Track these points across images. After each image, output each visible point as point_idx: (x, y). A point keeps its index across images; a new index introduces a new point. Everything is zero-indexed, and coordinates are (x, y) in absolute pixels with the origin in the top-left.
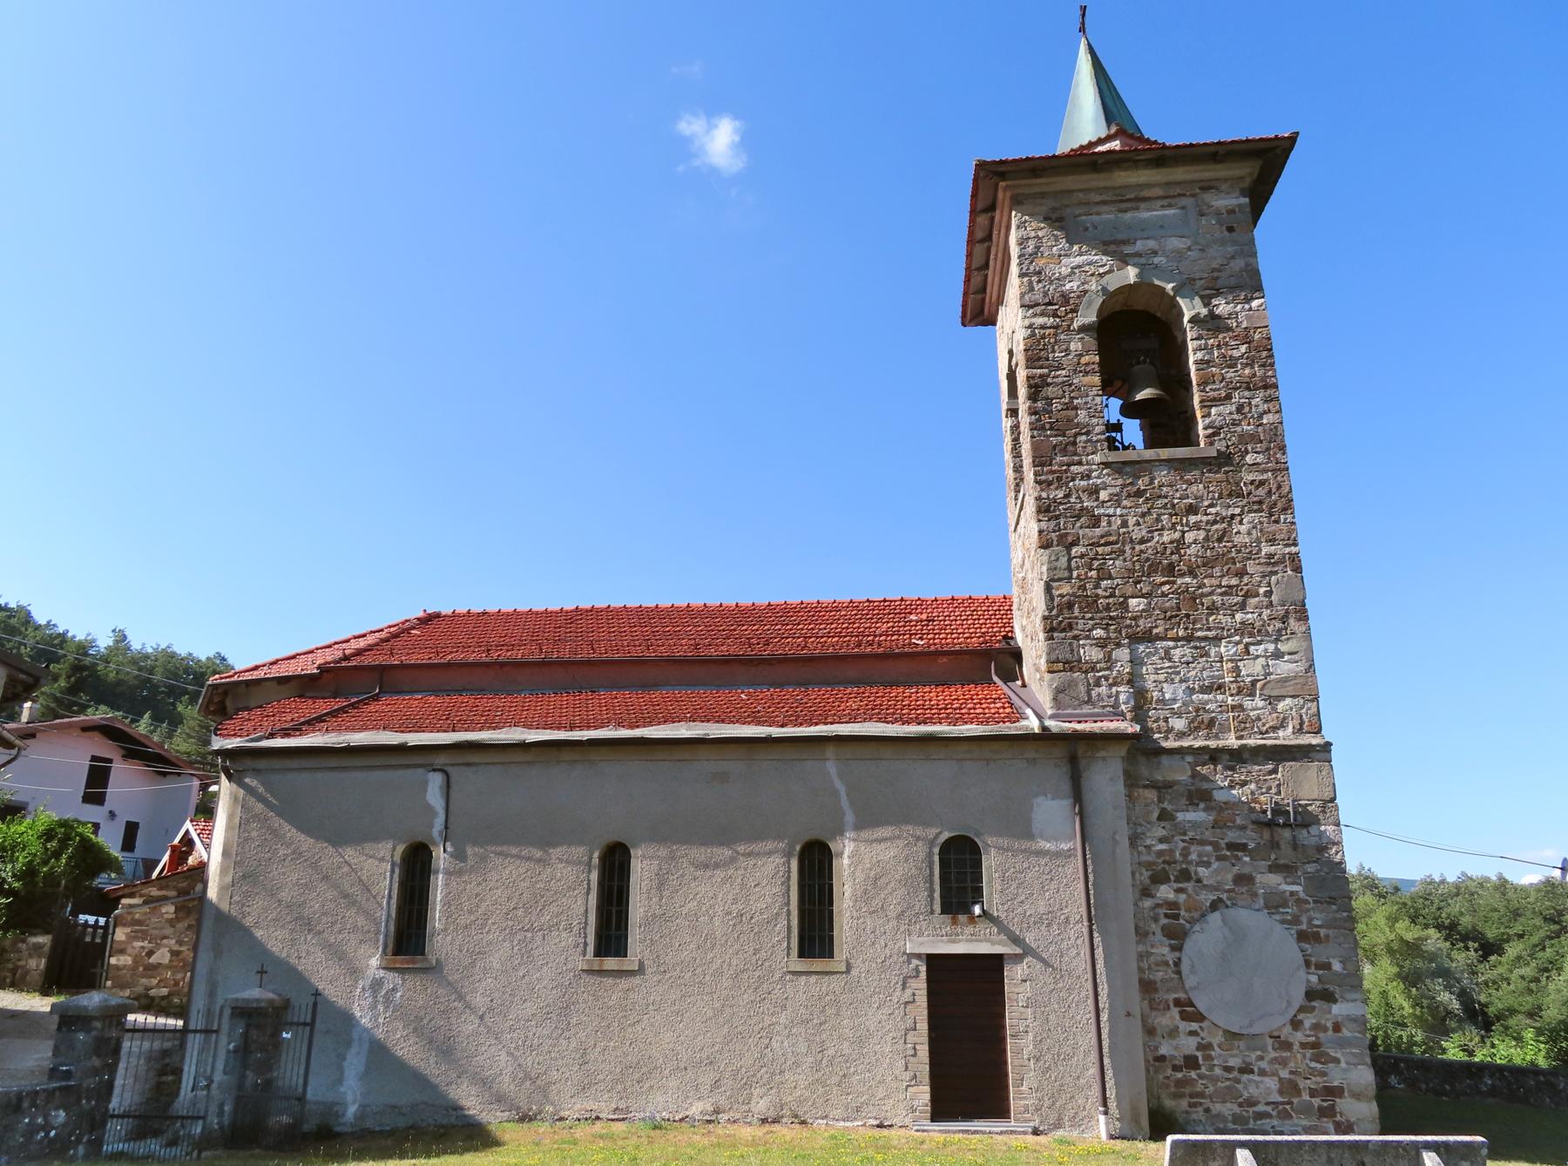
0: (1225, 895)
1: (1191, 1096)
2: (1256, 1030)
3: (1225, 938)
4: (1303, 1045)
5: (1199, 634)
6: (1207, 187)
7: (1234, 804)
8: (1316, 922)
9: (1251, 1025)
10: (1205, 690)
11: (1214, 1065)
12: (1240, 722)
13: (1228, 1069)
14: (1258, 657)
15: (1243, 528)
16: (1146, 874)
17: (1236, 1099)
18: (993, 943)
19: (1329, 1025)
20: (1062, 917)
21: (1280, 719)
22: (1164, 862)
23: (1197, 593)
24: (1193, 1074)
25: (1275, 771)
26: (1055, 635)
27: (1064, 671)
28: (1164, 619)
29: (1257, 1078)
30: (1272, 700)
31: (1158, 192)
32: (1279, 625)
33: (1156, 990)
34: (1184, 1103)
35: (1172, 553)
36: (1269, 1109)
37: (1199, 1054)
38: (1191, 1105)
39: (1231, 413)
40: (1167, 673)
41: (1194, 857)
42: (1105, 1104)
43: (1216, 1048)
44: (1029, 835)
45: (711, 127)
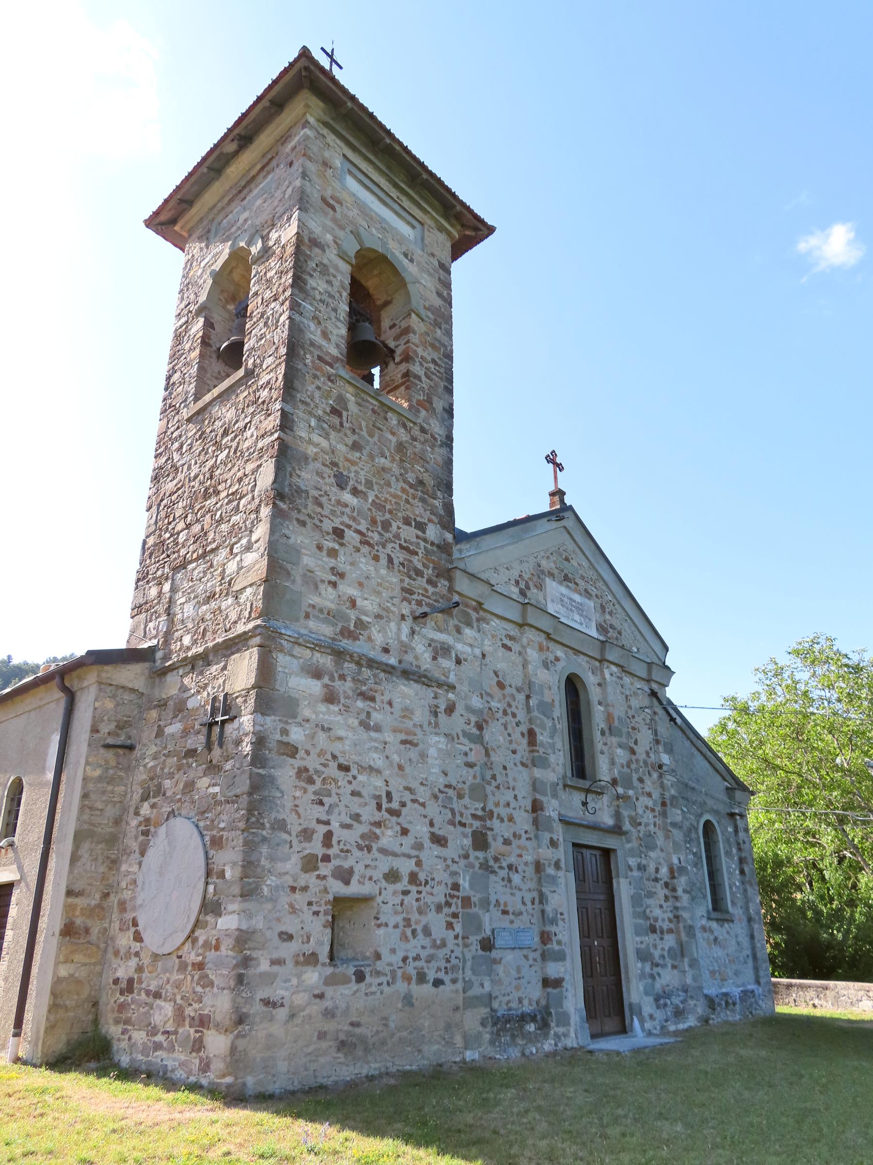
6: (284, 138)
7: (197, 709)
14: (237, 555)
25: (224, 668)
31: (259, 167)
42: (19, 1023)
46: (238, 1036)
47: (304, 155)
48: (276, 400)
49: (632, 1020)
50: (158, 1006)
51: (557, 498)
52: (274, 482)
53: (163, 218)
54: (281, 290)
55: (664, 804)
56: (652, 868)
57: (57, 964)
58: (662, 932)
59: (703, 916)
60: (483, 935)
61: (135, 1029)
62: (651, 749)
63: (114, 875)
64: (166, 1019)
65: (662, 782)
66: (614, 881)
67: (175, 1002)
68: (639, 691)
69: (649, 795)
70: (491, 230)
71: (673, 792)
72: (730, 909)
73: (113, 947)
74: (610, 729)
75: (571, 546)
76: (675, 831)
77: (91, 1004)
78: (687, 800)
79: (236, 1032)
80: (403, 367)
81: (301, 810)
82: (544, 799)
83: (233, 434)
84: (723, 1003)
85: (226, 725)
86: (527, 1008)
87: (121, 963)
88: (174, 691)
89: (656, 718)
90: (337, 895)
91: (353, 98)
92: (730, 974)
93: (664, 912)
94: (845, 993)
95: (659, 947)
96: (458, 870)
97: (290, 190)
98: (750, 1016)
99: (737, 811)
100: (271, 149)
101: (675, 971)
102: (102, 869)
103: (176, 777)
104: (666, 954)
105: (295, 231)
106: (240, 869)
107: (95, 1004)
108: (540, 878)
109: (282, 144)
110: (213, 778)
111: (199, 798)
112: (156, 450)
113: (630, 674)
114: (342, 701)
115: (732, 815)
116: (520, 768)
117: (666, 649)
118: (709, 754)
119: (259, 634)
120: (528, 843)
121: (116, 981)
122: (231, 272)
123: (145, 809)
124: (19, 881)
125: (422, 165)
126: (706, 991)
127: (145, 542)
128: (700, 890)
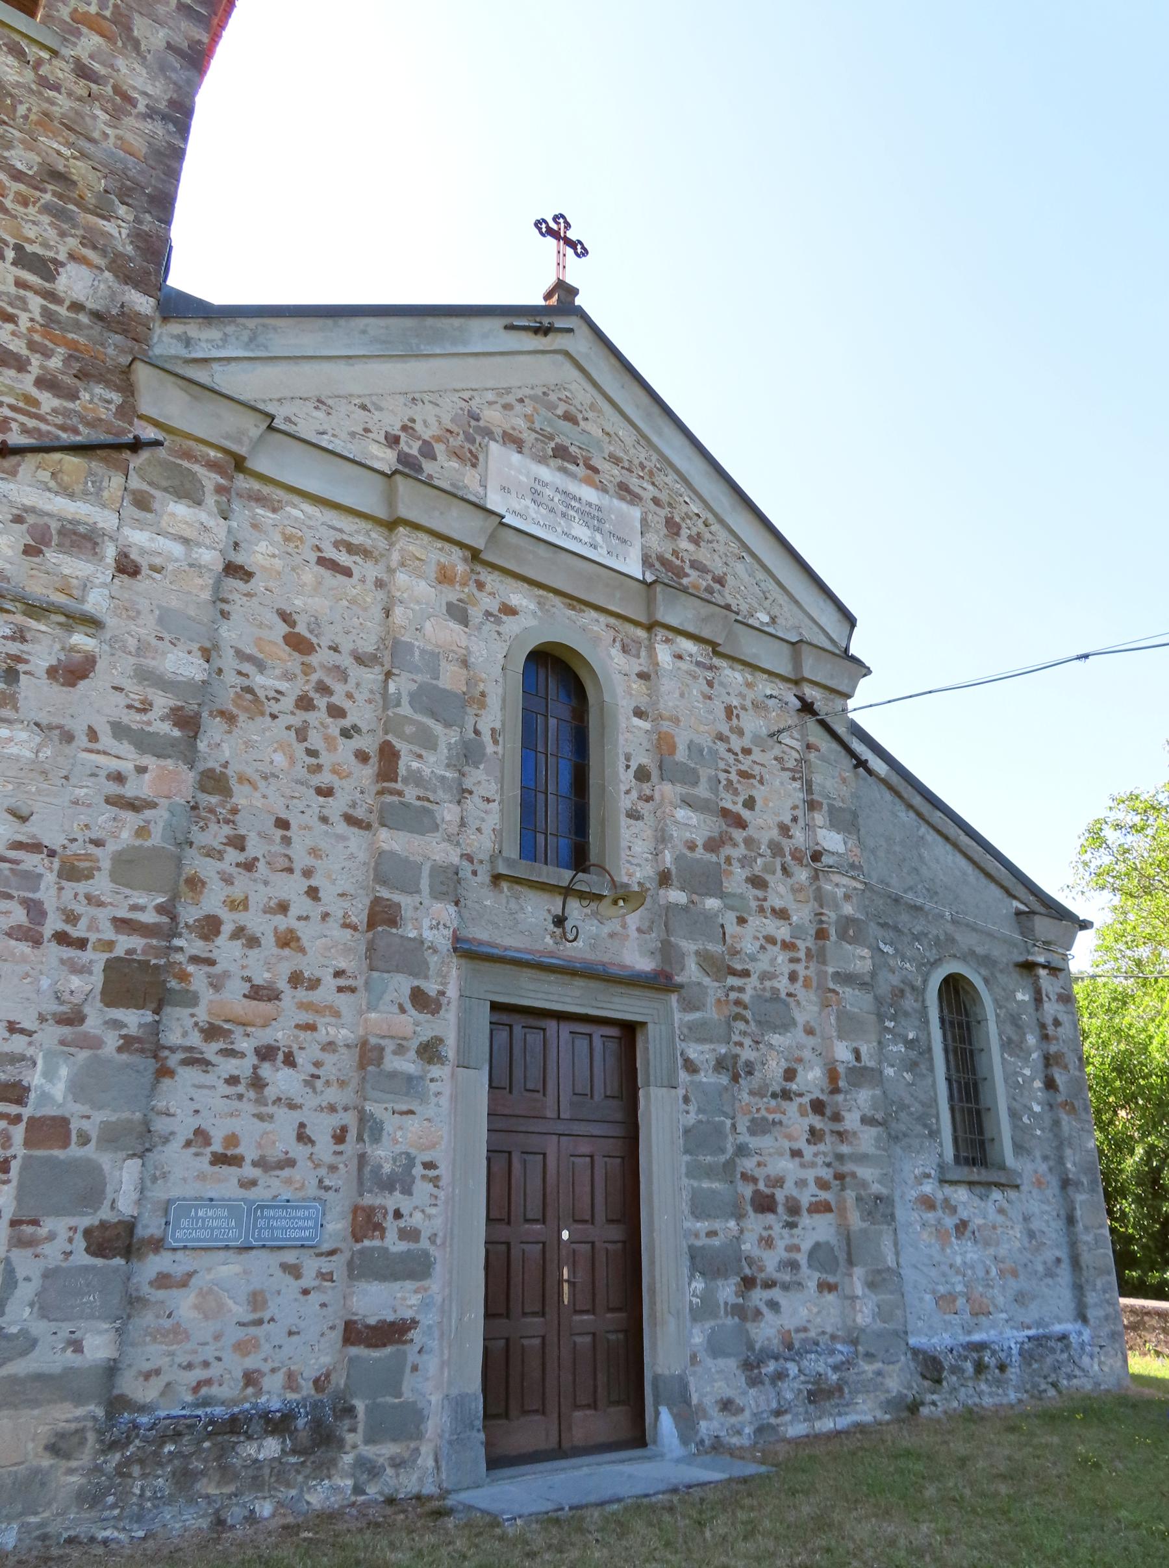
55: (821, 935)
56: (774, 1068)
58: (794, 1209)
59: (928, 1176)
60: (105, 1214)
62: (795, 819)
65: (819, 889)
66: (641, 1093)
68: (771, 703)
69: (782, 914)
71: (848, 909)
72: (1010, 1160)
74: (660, 768)
75: (582, 394)
76: (848, 993)
78: (896, 929)
82: (405, 901)
84: (969, 1366)
86: (273, 1395)
89: (812, 756)
92: (1000, 1300)
93: (803, 1166)
95: (780, 1245)
96: (29, 1052)
98: (1052, 1392)
99: (1041, 959)
101: (830, 1297)
104: (802, 1258)
113: (745, 664)
115: (1028, 967)
116: (342, 827)
117: (850, 621)
118: (964, 839)
120: (343, 1001)
126: (912, 1341)
128: (921, 1119)
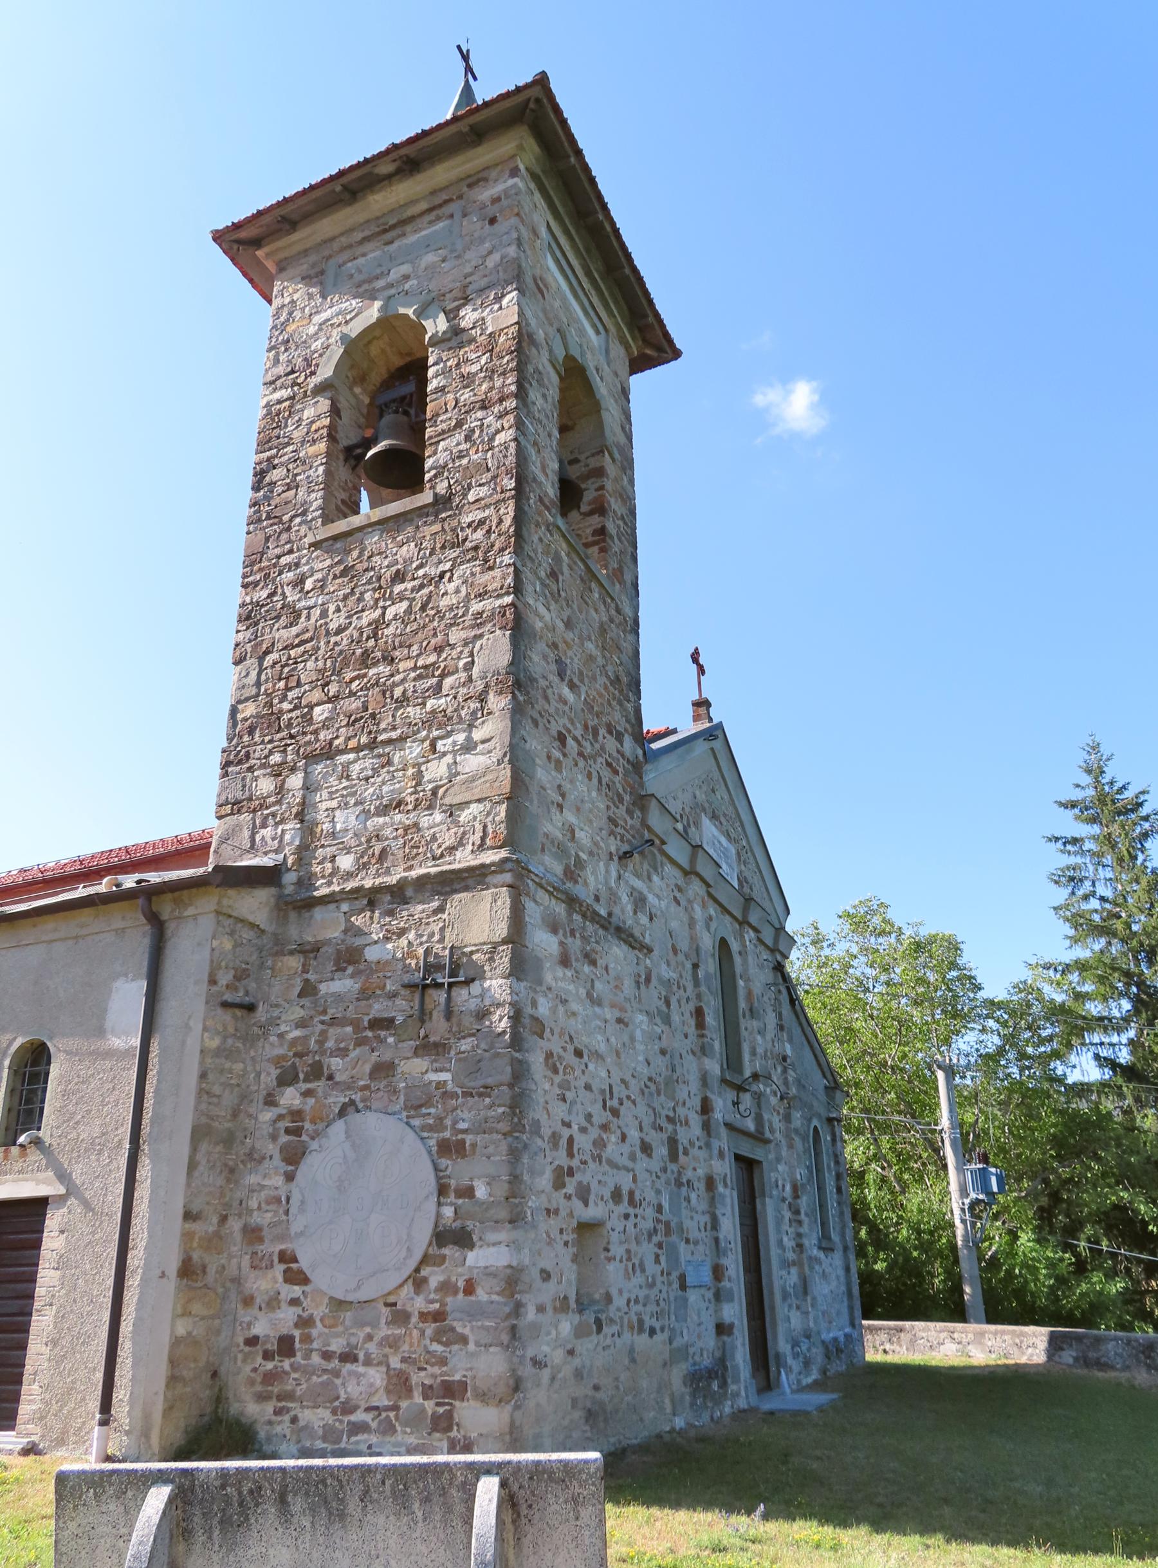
0: (359, 1094)
1: (280, 1398)
2: (362, 1295)
3: (345, 1157)
4: (423, 1316)
5: (383, 737)
6: (476, 180)
7: (387, 962)
8: (463, 1126)
9: (359, 1287)
10: (383, 810)
11: (312, 1350)
12: (413, 847)
13: (327, 1356)
14: (444, 754)
15: (451, 587)
16: (275, 1073)
17: (331, 1402)
18: (38, 1182)
19: (461, 1284)
20: (116, 1139)
21: (459, 835)
22: (295, 1055)
23: (388, 683)
24: (286, 1364)
25: (441, 909)
26: (230, 769)
27: (232, 814)
28: (348, 725)
29: (361, 1369)
30: (451, 812)
31: (424, 206)
32: (474, 705)
33: (261, 1240)
34: (269, 1407)
35: (368, 638)
36: (367, 1417)
37: (297, 1333)
38: (278, 1412)
39: (458, 444)
40: (342, 796)
41: (330, 1044)
42: (106, 1405)
43: (318, 1323)
44: (100, 1032)
45: (789, 392)
46: (517, 1407)
47: (518, 214)
48: (502, 550)
49: (779, 1373)
50: (350, 1373)
51: (702, 710)
52: (512, 664)
53: (243, 234)
54: (494, 395)
57: (175, 1317)
61: (302, 1407)
63: (231, 1190)
64: (373, 1390)
66: (758, 1201)
67: (388, 1366)
70: (677, 354)
73: (241, 1292)
77: (209, 1375)
79: (513, 1403)
80: (595, 521)
81: (549, 1107)
83: (416, 583)
85: (454, 989)
87: (260, 1315)
88: (334, 933)
90: (582, 1220)
91: (579, 153)
94: (924, 1335)
97: (496, 257)
100: (447, 187)
102: (220, 1181)
103: (353, 1055)
105: (515, 319)
106: (506, 1186)
107: (215, 1374)
108: (713, 1198)
109: (470, 186)
110: (435, 1061)
111: (407, 1087)
112: (245, 576)
114: (574, 964)
117: (788, 913)
119: (510, 870)
121: (252, 1341)
122: (369, 342)
123: (290, 1097)
124: (62, 1199)
125: (628, 256)
127: (234, 711)
